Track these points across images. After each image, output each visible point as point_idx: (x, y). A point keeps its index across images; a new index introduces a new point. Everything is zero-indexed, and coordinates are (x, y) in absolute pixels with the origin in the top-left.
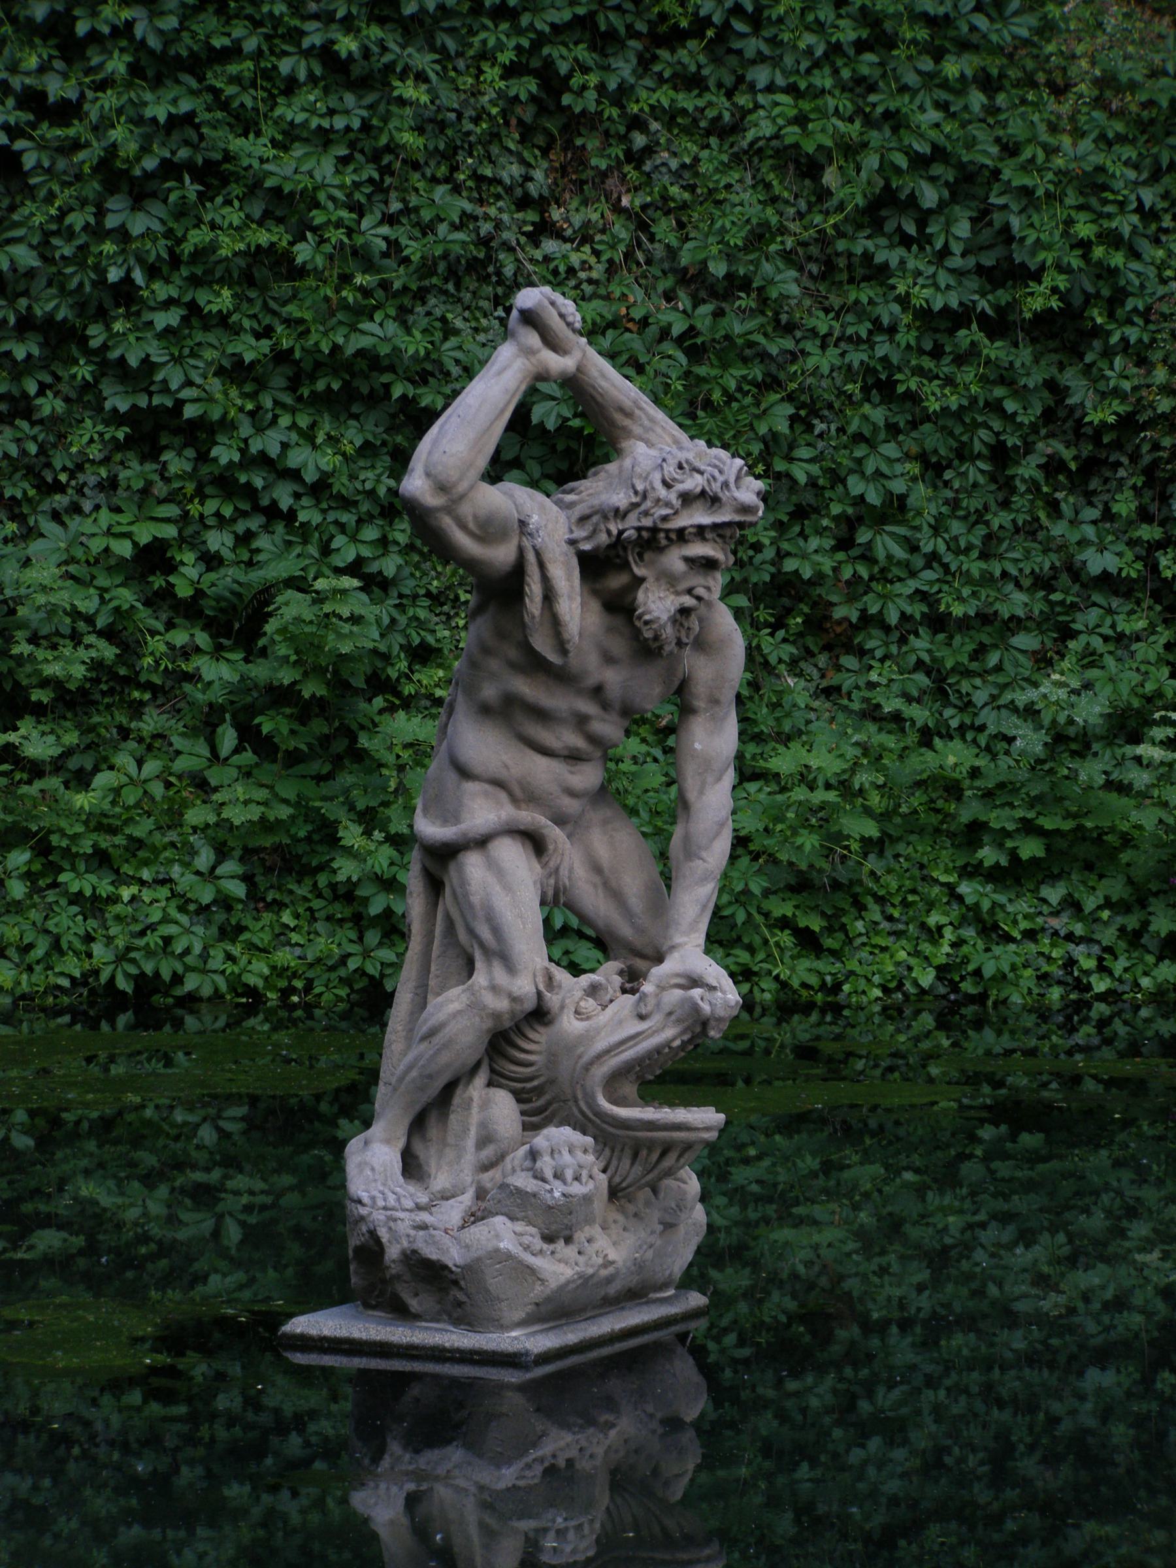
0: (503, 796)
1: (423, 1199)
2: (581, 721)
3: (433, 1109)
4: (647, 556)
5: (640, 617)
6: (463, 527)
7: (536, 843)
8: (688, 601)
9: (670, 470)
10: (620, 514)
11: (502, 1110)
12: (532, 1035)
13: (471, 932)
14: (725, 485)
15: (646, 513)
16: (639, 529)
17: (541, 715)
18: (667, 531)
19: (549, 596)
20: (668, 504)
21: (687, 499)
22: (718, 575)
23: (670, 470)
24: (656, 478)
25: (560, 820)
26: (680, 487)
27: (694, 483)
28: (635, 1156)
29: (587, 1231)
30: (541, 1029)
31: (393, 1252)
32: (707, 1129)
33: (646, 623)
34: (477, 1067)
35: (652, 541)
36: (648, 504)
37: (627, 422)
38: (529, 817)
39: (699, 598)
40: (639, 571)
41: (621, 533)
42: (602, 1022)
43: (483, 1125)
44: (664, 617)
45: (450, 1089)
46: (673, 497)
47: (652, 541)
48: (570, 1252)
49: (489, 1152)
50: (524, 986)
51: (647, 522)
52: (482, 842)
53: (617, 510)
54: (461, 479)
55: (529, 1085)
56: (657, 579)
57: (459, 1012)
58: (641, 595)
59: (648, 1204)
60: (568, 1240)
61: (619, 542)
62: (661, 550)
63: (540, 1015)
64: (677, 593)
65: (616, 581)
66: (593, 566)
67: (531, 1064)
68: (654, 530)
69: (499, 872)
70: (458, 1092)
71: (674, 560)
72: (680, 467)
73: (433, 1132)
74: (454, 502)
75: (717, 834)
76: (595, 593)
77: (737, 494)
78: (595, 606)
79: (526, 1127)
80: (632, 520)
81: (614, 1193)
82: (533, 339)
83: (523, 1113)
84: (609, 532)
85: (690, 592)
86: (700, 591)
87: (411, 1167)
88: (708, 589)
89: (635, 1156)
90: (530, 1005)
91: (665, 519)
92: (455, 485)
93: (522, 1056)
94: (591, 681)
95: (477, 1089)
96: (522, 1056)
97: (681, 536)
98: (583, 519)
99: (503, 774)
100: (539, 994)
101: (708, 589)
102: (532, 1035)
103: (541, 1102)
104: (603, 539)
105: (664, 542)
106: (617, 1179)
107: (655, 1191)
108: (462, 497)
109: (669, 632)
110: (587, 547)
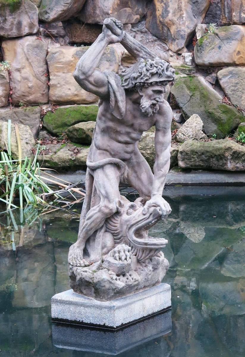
0: (108, 153)
1: (87, 263)
2: (128, 134)
3: (89, 240)
4: (143, 89)
5: (141, 106)
6: (91, 83)
7: (117, 166)
8: (155, 102)
9: (148, 67)
10: (135, 79)
11: (108, 239)
12: (116, 218)
13: (100, 191)
14: (163, 71)
15: (142, 78)
16: (140, 83)
17: (118, 133)
18: (148, 83)
19: (116, 101)
20: (147, 76)
21: (153, 75)
22: (163, 95)
23: (148, 67)
24: (144, 69)
25: (124, 160)
26: (151, 71)
27: (154, 70)
28: (143, 251)
29: (130, 273)
30: (118, 217)
31: (78, 278)
32: (162, 245)
33: (143, 108)
34: (102, 228)
35: (144, 86)
36: (142, 76)
37: (138, 53)
38: (117, 160)
39: (157, 101)
40: (141, 94)
41: (136, 83)
42: (136, 213)
43: (103, 243)
44: (147, 106)
45: (96, 232)
46: (148, 74)
47: (144, 86)
48: (124, 279)
49: (105, 250)
50: (113, 206)
51: (142, 81)
52: (102, 167)
53: (134, 77)
54: (89, 71)
55: (116, 232)
56: (146, 96)
57: (96, 213)
58: (141, 100)
59: (149, 263)
60: (124, 275)
61: (135, 86)
62: (147, 88)
63: (118, 213)
64: (151, 100)
65: (136, 96)
66: (129, 92)
67: (116, 227)
68: (144, 83)
69: (107, 176)
70: (98, 233)
71: (150, 91)
72: (151, 65)
73: (91, 244)
74: (87, 77)
75: (165, 164)
76: (130, 99)
77: (166, 73)
78: (130, 102)
79: (115, 243)
80: (138, 80)
81: (138, 261)
82: (110, 33)
83: (115, 239)
84: (132, 83)
85: (155, 99)
86: (157, 99)
87: (86, 253)
88: (159, 98)
89: (143, 251)
90: (114, 211)
91: (147, 80)
92: (87, 73)
93: (114, 224)
94: (130, 123)
95: (101, 234)
96: (114, 224)
97: (151, 84)
98: (126, 80)
99: (108, 148)
100: (117, 208)
101: (159, 98)
102: (116, 218)
103: (119, 236)
104: (130, 85)
105: (147, 86)
106: (139, 258)
107: (151, 260)
108: (90, 76)
109: (150, 110)
110: (126, 87)
